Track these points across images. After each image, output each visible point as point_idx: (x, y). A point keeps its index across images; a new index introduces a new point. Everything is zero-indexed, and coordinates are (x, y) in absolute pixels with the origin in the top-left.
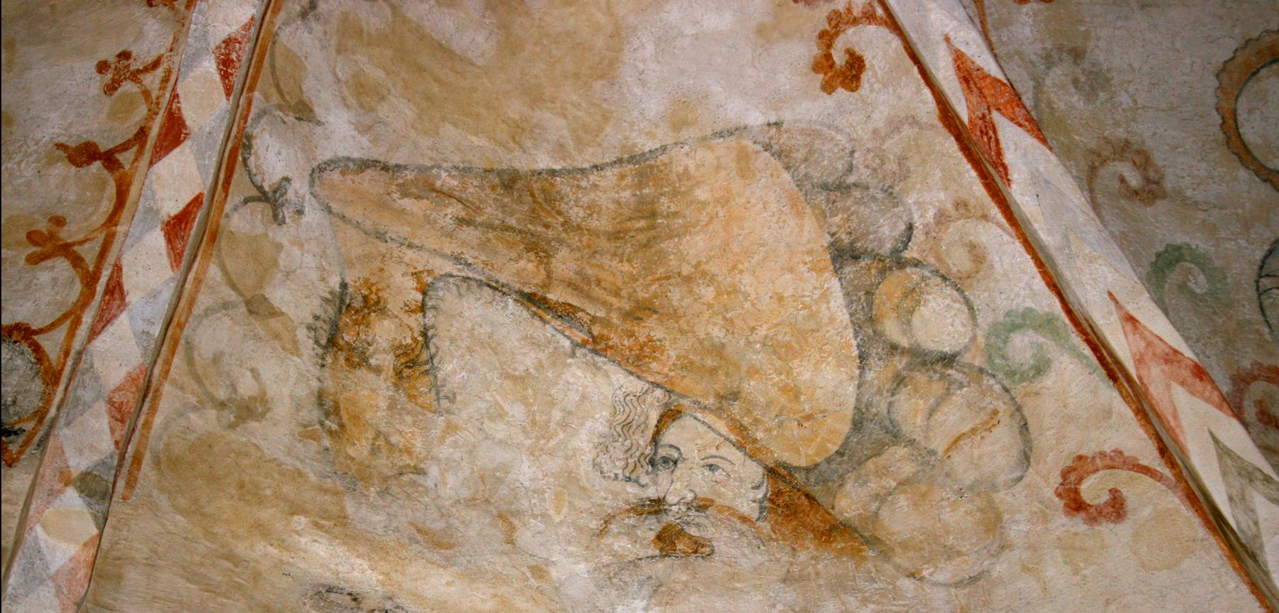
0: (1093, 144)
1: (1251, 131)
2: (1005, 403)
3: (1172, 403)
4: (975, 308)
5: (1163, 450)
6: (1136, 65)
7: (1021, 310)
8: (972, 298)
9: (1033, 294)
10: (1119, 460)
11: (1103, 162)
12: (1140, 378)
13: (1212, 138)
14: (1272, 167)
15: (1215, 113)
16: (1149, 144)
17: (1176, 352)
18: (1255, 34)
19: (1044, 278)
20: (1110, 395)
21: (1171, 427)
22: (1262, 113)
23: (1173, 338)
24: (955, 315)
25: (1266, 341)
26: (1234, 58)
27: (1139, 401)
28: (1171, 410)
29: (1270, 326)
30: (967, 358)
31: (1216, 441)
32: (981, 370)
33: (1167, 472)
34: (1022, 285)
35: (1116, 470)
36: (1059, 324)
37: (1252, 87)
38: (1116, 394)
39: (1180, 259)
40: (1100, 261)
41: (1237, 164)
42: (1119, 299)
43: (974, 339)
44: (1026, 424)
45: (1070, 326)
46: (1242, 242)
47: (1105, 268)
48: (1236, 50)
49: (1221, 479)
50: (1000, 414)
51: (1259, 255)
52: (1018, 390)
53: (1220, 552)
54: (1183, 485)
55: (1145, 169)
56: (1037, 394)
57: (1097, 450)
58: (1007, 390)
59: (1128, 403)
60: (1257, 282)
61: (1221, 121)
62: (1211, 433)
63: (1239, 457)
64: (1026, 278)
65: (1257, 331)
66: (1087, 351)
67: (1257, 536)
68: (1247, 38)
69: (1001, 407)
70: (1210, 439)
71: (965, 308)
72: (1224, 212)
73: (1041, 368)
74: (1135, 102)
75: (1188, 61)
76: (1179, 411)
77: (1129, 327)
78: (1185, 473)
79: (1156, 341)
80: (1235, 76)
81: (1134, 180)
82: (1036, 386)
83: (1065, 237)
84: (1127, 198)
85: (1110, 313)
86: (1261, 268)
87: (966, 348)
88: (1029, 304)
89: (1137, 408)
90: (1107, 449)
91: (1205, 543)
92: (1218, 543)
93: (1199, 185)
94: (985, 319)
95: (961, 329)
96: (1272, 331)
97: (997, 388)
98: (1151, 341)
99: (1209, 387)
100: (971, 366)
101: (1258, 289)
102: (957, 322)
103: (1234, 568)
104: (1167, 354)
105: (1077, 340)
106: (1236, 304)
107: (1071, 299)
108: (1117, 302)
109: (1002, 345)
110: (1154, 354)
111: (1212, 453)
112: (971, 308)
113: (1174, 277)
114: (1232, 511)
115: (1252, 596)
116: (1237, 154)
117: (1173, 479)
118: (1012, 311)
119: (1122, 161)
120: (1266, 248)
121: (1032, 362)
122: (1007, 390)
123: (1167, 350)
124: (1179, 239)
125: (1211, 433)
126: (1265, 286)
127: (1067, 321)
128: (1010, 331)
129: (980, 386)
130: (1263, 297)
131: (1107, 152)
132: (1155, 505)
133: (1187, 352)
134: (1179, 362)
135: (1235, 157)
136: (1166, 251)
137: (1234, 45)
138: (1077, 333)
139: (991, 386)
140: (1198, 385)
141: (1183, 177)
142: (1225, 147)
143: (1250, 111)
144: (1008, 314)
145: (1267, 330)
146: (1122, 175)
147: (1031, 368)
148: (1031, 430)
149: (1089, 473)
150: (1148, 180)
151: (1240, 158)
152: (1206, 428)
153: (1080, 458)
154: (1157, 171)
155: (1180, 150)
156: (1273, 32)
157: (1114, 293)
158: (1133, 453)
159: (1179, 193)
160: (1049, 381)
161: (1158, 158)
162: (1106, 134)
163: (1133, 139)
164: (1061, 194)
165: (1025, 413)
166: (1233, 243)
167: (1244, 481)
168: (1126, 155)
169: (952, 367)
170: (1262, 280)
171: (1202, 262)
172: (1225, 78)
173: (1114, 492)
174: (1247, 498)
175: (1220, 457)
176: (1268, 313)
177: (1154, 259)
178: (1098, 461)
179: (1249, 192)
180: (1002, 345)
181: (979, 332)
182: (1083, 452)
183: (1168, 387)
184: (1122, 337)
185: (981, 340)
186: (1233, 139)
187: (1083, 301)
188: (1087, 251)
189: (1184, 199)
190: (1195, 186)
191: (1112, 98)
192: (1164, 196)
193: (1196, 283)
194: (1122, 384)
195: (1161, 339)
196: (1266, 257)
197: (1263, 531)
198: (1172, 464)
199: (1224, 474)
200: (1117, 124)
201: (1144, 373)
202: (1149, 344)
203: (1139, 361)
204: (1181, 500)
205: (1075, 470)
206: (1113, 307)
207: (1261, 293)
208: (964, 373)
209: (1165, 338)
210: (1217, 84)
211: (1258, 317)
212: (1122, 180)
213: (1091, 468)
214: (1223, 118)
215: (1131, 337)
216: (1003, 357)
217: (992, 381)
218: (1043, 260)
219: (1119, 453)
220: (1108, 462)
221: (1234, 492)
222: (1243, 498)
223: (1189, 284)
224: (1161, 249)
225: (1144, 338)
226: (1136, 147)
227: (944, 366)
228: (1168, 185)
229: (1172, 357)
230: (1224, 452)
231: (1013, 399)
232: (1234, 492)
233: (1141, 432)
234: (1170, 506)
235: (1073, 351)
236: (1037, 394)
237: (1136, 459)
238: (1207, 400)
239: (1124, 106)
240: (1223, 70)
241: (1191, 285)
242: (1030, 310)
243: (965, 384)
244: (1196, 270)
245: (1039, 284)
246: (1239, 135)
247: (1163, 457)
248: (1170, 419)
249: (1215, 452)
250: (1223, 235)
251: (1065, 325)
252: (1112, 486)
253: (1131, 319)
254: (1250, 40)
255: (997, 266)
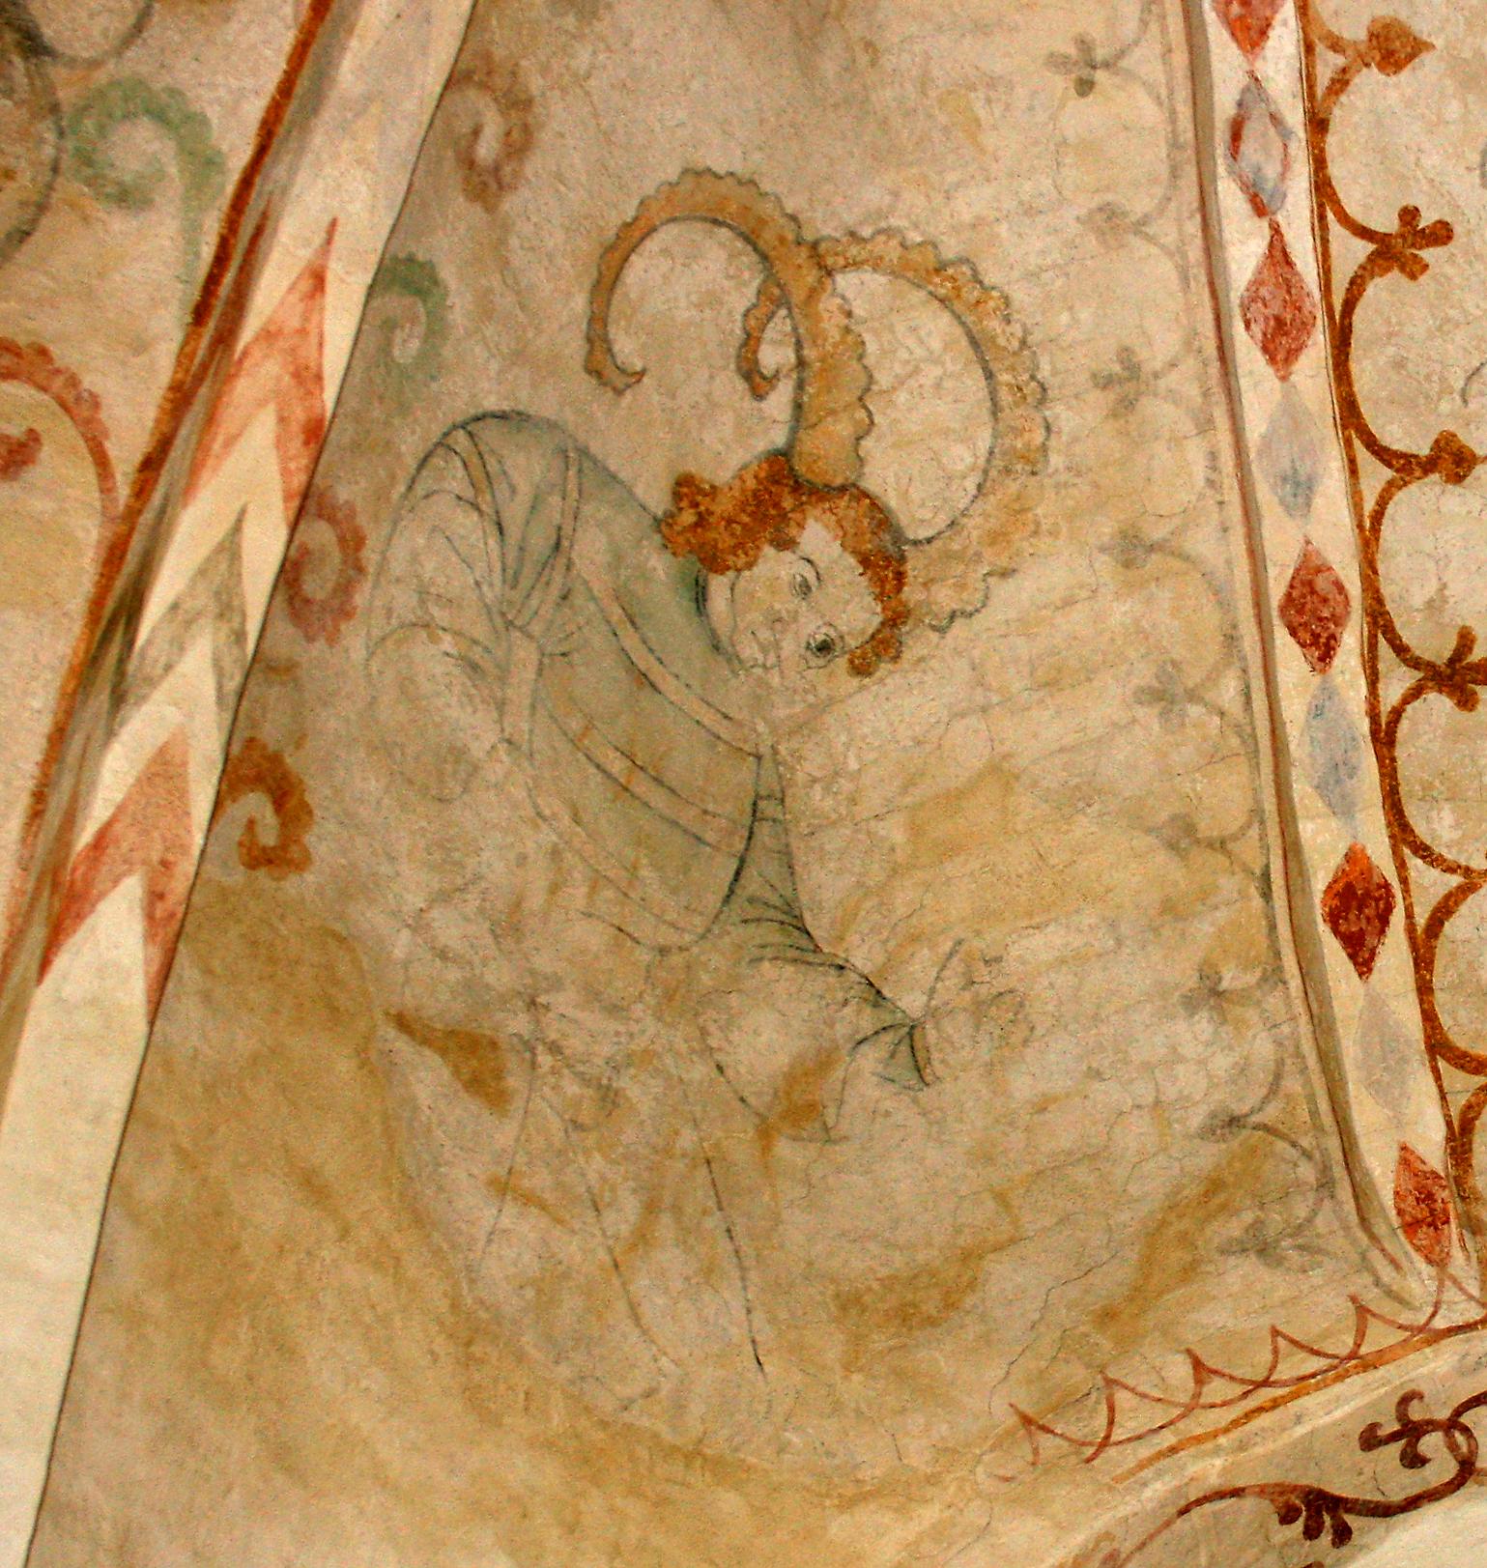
0: (499, 53)
1: (640, 271)
2: (33, 180)
3: (244, 426)
4: (145, 35)
5: (151, 465)
6: (636, 43)
7: (195, 107)
8: (156, 19)
9: (233, 110)
10: (85, 412)
11: (484, 86)
12: (245, 353)
13: (602, 224)
14: (611, 336)
15: (636, 202)
16: (545, 137)
17: (319, 378)
18: (766, 186)
19: (268, 110)
20: (168, 327)
21: (209, 449)
22: (672, 269)
23: (334, 361)
24: (111, 11)
25: (388, 499)
26: (721, 178)
27: (199, 379)
28: (233, 431)
29: (410, 488)
30: (57, 73)
31: (237, 528)
32: (55, 109)
33: (123, 492)
34: (234, 83)
35: (66, 419)
36: (217, 179)
37: (696, 231)
38: (178, 336)
39: (421, 293)
40: (369, 175)
41: (587, 284)
42: (337, 238)
43: (95, 64)
44: (28, 234)
45: (225, 200)
46: (494, 366)
47: (364, 189)
48: (732, 174)
49: (191, 573)
50: (14, 185)
51: (491, 403)
52: (70, 187)
53: (69, 651)
54: (123, 528)
55: (509, 155)
56: (85, 219)
57: (73, 368)
58: (55, 169)
59: (179, 363)
60: (455, 427)
61: (629, 220)
62: (243, 512)
63: (240, 575)
64: (249, 83)
65: (393, 477)
66: (208, 251)
67: (152, 682)
68: (756, 177)
69: (25, 178)
70: (233, 518)
71: (131, 20)
72: (518, 312)
73: (129, 198)
74: (588, 76)
75: (682, 115)
76: (242, 442)
77: (306, 285)
78: (148, 517)
79: (314, 340)
80: (699, 198)
81: (487, 150)
82: (98, 210)
83: (369, 98)
84: (458, 153)
85: (307, 243)
86: (477, 419)
87: (72, 63)
88: (214, 114)
89: (182, 383)
90: (88, 381)
91: (65, 621)
92: (80, 640)
93: (532, 249)
94: (138, 61)
95: (96, 32)
96: (405, 497)
97: (48, 151)
98: (308, 332)
99: (304, 462)
100: (50, 89)
101: (446, 435)
102: (103, 20)
103: (63, 687)
104: (307, 368)
105: (212, 226)
106: (410, 419)
107: (277, 170)
108: (329, 241)
109: (118, 113)
110: (293, 350)
111: (219, 532)
112: (139, 28)
113: (393, 303)
114: (162, 620)
115: (43, 743)
116: (600, 273)
117: (121, 508)
118: (181, 94)
119: (502, 113)
120: (506, 406)
121: (128, 178)
122: (55, 169)
123: (312, 364)
124: (447, 273)
125: (243, 512)
126: (457, 443)
127: (230, 189)
128: (148, 112)
129: (31, 124)
130: (441, 451)
131: (500, 82)
132: (62, 511)
133: (330, 395)
134: (310, 393)
135: (595, 274)
136: (422, 266)
137: (738, 168)
138: (222, 216)
139: (42, 141)
140: (296, 444)
141: (529, 219)
142: (601, 250)
143: (666, 252)
144: (173, 92)
145: (402, 489)
146: (482, 126)
147: (119, 184)
148: (25, 248)
149: (30, 380)
150: (497, 169)
151: (598, 282)
152: (244, 498)
153: (43, 352)
154: (516, 174)
155: (562, 189)
156: (782, 209)
157: (339, 229)
158: (109, 423)
159: (506, 228)
160: (119, 224)
161: (535, 165)
162: (524, 63)
163: (537, 109)
164: (424, 50)
165: (46, 222)
166: (486, 355)
167: (213, 608)
168: (513, 113)
169: (26, 59)
170: (461, 432)
171: (436, 330)
172: (688, 184)
173: (33, 437)
174: (194, 627)
175: (220, 549)
176: (424, 473)
177: (402, 255)
178: (58, 382)
179: (561, 328)
180: (118, 113)
181: (111, 65)
182: (55, 351)
183: (262, 404)
184: (285, 284)
185: (101, 77)
186: (617, 255)
187: (296, 190)
188: (370, 146)
189: (502, 242)
190: (526, 245)
191: (574, 37)
192: (491, 209)
193: (405, 341)
194: (200, 336)
195: (321, 345)
196: (494, 416)
197: (165, 685)
198: (142, 490)
199: (202, 572)
200: (545, 70)
201: (257, 353)
202: (302, 332)
203: (268, 335)
204: (99, 542)
205: (18, 355)
206: (318, 240)
207: (443, 444)
208: (32, 84)
209: (328, 349)
210: (674, 178)
211: (412, 463)
212: (476, 132)
213: (41, 377)
214: (636, 219)
215: (294, 298)
216: (102, 129)
217: (50, 136)
218: (298, 90)
219: (95, 403)
220: (70, 398)
221: (188, 604)
222: (188, 623)
223: (398, 332)
224: (421, 257)
225: (306, 317)
226: (530, 120)
227: (19, 44)
228: (510, 204)
229: (308, 378)
230: (230, 548)
231: (50, 187)
232: (188, 604)
233: (151, 414)
234: (80, 534)
235: (191, 233)
236: (85, 219)
237: (107, 437)
238: (285, 472)
239: (573, 64)
240: (698, 174)
241: (399, 336)
242: (204, 122)
243: (16, 96)
244: (420, 329)
245: (255, 110)
246: (626, 259)
247: (277, 447)
248: (220, 439)
249: (221, 536)
250: (488, 334)
251: (222, 187)
252: (38, 427)
253: (318, 280)
254: (755, 184)
255: (234, 26)
